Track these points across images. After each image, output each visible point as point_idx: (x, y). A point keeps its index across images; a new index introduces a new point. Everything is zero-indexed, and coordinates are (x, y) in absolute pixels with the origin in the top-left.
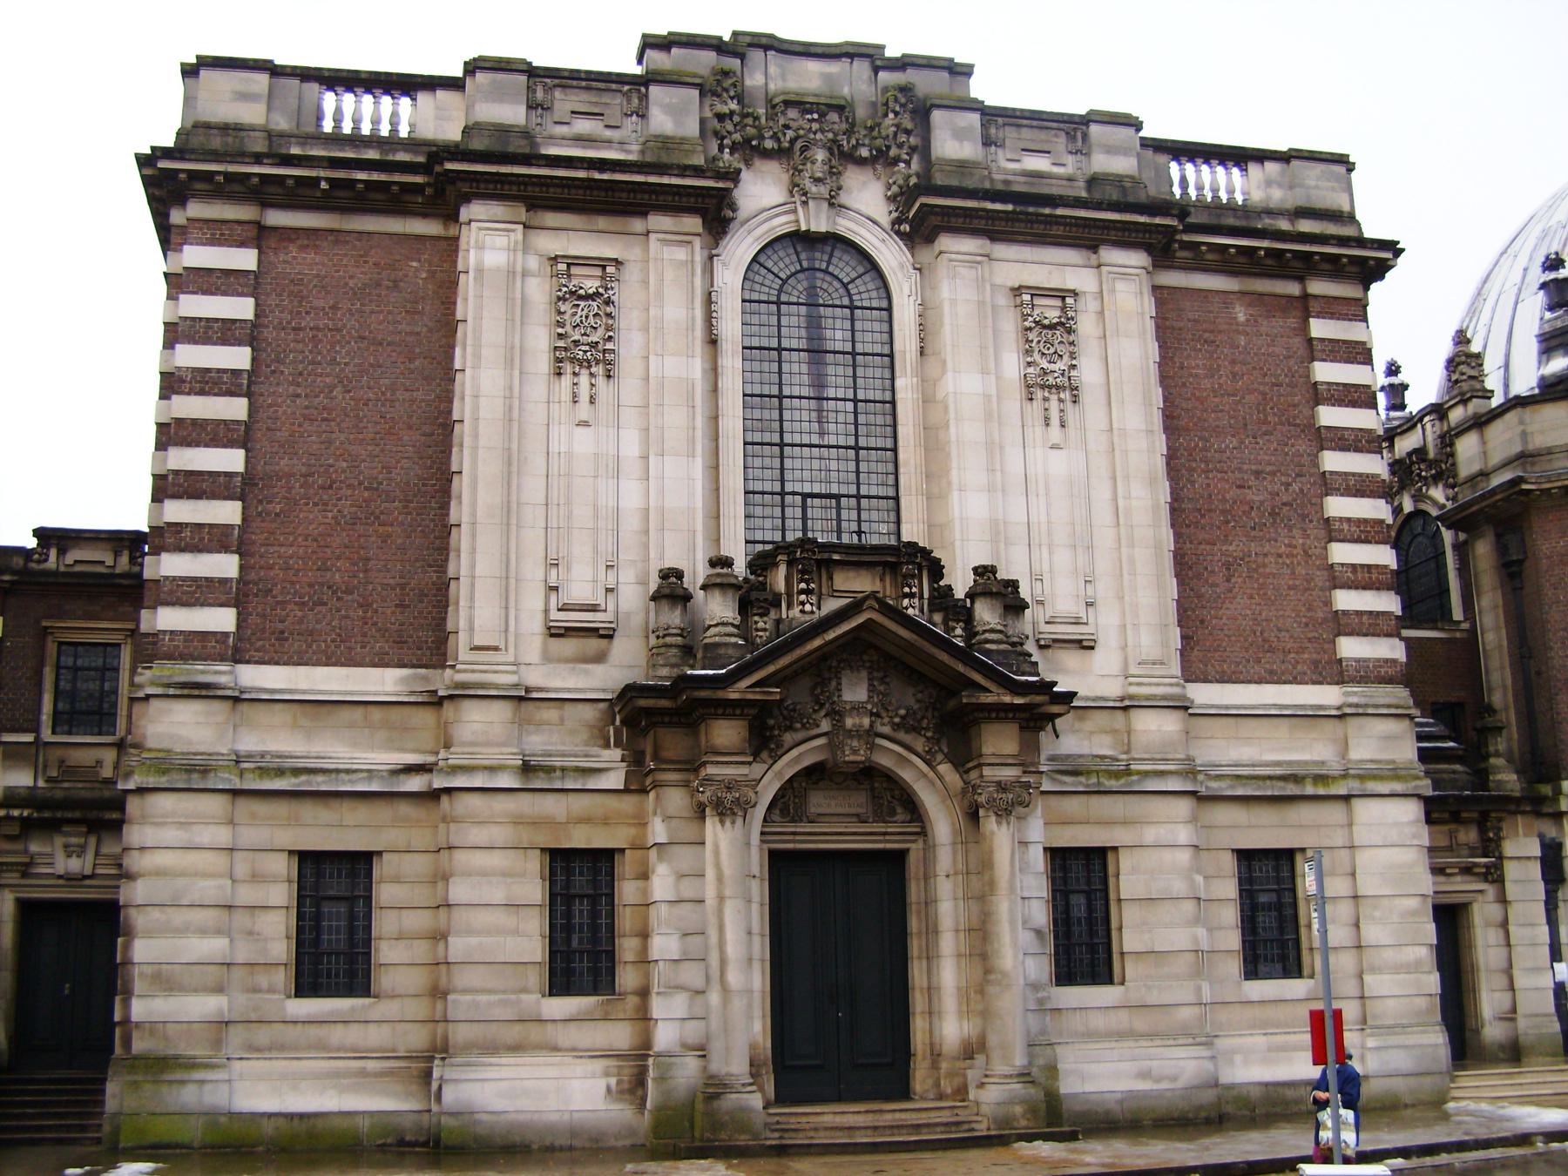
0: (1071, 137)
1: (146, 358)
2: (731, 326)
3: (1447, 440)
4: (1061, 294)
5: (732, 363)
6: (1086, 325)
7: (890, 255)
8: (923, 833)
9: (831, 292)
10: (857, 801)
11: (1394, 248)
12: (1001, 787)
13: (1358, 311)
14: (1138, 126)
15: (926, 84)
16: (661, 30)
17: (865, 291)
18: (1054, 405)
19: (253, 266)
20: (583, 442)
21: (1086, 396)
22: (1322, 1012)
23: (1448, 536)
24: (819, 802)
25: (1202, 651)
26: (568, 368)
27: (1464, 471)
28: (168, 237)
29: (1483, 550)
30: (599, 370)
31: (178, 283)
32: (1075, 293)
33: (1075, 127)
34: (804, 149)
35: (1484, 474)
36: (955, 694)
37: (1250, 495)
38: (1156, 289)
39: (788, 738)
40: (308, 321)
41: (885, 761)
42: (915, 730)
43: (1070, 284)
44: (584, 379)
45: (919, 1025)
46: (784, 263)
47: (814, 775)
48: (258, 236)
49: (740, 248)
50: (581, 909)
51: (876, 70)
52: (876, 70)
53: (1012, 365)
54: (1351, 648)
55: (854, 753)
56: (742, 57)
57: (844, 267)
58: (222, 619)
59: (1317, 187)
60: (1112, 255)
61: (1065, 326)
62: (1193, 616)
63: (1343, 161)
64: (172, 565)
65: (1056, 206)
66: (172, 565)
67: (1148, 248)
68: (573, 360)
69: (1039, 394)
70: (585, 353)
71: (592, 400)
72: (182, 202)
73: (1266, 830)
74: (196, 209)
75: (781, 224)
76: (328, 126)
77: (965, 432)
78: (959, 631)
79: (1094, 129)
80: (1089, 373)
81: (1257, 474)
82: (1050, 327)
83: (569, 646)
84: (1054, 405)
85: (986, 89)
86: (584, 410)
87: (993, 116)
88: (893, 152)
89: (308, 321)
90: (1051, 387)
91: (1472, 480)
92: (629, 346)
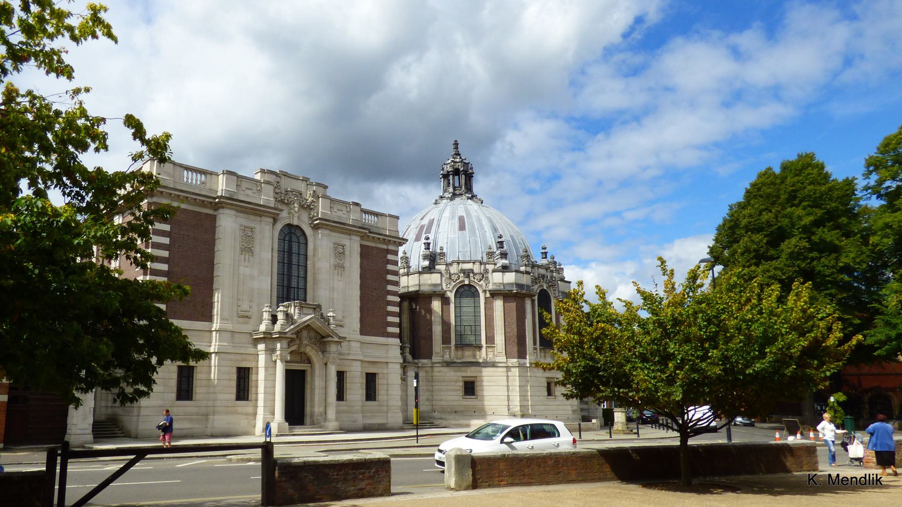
6: (347, 252)
7: (308, 231)
9: (294, 239)
16: (265, 168)
17: (302, 240)
20: (247, 271)
22: (397, 255)
38: (362, 246)
40: (182, 232)
50: (242, 380)
54: (390, 330)
57: (298, 233)
60: (354, 237)
61: (343, 253)
65: (449, 325)
70: (247, 248)
73: (371, 370)
75: (287, 221)
80: (347, 265)
82: (340, 252)
83: (241, 320)
89: (182, 232)
91: (404, 287)
92: (256, 249)
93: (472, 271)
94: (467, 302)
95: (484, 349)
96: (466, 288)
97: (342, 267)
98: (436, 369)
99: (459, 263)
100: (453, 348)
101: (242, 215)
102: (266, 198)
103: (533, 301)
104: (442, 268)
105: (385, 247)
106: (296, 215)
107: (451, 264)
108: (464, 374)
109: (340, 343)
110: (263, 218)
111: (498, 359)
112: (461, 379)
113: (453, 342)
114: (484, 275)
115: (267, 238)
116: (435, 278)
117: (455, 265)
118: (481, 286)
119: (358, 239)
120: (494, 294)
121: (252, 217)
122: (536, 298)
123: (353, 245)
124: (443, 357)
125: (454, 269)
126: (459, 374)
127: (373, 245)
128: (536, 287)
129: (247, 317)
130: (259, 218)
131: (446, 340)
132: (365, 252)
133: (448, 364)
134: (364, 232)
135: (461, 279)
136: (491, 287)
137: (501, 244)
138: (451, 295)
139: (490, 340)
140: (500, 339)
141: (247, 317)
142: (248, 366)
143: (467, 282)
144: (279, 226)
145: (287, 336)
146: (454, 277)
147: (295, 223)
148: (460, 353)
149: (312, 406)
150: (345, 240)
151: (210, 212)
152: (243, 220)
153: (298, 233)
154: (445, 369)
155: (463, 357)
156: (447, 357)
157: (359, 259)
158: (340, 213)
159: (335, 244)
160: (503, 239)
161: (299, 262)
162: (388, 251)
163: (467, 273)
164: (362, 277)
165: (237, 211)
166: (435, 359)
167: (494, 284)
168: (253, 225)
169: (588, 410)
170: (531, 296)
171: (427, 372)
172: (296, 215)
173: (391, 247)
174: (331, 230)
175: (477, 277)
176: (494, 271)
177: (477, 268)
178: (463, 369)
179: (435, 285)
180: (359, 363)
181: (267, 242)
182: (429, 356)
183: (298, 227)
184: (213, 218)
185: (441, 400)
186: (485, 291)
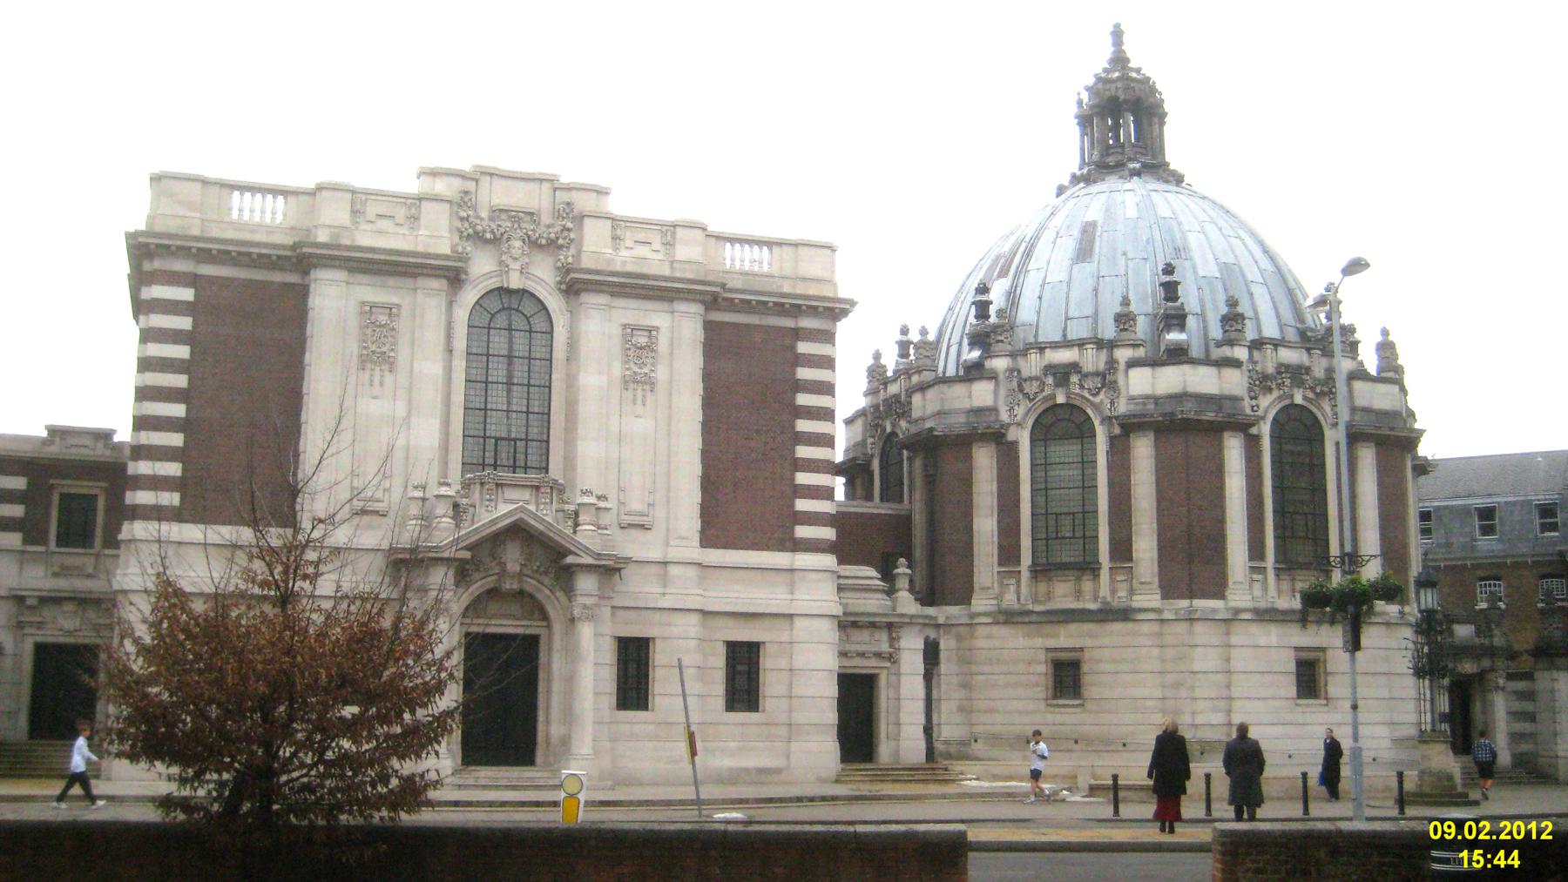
0: (664, 234)
1: (129, 378)
2: (460, 343)
3: (910, 392)
4: (650, 330)
5: (460, 364)
7: (554, 302)
8: (549, 627)
10: (514, 608)
11: (853, 303)
12: (585, 607)
13: (828, 337)
14: (704, 229)
15: (583, 202)
17: (539, 323)
18: (639, 393)
19: (179, 473)
21: (659, 387)
23: (905, 453)
24: (493, 607)
25: (719, 526)
26: (369, 365)
27: (916, 414)
28: (140, 307)
29: (918, 463)
30: (386, 367)
31: (147, 336)
32: (657, 329)
33: (669, 231)
34: (509, 239)
35: (923, 419)
36: (565, 556)
37: (752, 444)
38: (709, 326)
39: (477, 576)
41: (528, 588)
42: (546, 573)
43: (656, 324)
44: (377, 373)
45: (541, 728)
46: (494, 305)
47: (493, 593)
48: (191, 280)
49: (470, 296)
51: (555, 190)
52: (555, 190)
53: (617, 369)
55: (509, 585)
56: (477, 181)
58: (171, 499)
59: (811, 265)
60: (681, 307)
61: (650, 348)
62: (709, 513)
63: (832, 249)
64: (143, 468)
66: (143, 468)
67: (703, 302)
68: (372, 361)
69: (632, 386)
71: (381, 384)
72: (150, 283)
74: (157, 264)
75: (493, 283)
76: (235, 215)
77: (588, 409)
78: (166, 696)
79: (680, 232)
80: (661, 374)
81: (758, 432)
82: (639, 347)
84: (639, 393)
85: (616, 205)
86: (377, 390)
87: (618, 224)
88: (560, 241)
90: (638, 382)
92: (403, 355)
93: (1075, 367)
94: (1065, 451)
95: (1105, 574)
96: (1065, 414)
97: (650, 383)
98: (981, 631)
99: (1042, 350)
100: (1025, 575)
101: (360, 277)
102: (435, 236)
103: (1252, 444)
104: (1000, 364)
105: (789, 323)
106: (516, 266)
107: (1024, 353)
108: (1052, 643)
109: (619, 570)
110: (423, 282)
111: (1139, 601)
112: (1042, 656)
113: (1026, 559)
114: (1107, 379)
115: (433, 335)
116: (981, 393)
117: (1034, 357)
118: (1096, 407)
119: (696, 308)
120: (1129, 427)
121: (392, 281)
122: (1265, 429)
123: (680, 332)
124: (999, 597)
125: (1032, 365)
126: (1039, 642)
127: (753, 320)
128: (1265, 401)
129: (642, 527)
130: (408, 282)
131: (1008, 553)
132: (720, 344)
133: (1008, 617)
134: (712, 297)
135: (1047, 391)
136: (1123, 407)
137: (1171, 290)
138: (1022, 438)
139: (1122, 550)
140: (1145, 547)
141: (642, 527)
142: (830, 689)
143: (1061, 399)
144: (470, 296)
145: (446, 555)
146: (1030, 388)
147: (515, 282)
148: (1042, 587)
149: (548, 722)
150: (657, 317)
151: (293, 278)
152: (371, 291)
153: (528, 307)
154: (1004, 631)
155: (1049, 596)
156: (1010, 599)
157: (698, 361)
158: (644, 251)
159: (625, 326)
160: (1175, 278)
161: (510, 376)
162: (798, 334)
163: (1062, 374)
164: (709, 403)
165: (351, 270)
166: (980, 603)
167: (1131, 398)
168: (395, 300)
169: (1532, 736)
170: (1243, 427)
171: (959, 638)
172: (516, 266)
173: (807, 323)
174: (613, 294)
175: (1089, 384)
176: (1132, 364)
177: (1092, 360)
178: (1048, 628)
179: (979, 411)
180: (694, 619)
181: (432, 335)
182: (964, 595)
183: (523, 293)
184: (303, 292)
185: (992, 711)
186: (1107, 420)
